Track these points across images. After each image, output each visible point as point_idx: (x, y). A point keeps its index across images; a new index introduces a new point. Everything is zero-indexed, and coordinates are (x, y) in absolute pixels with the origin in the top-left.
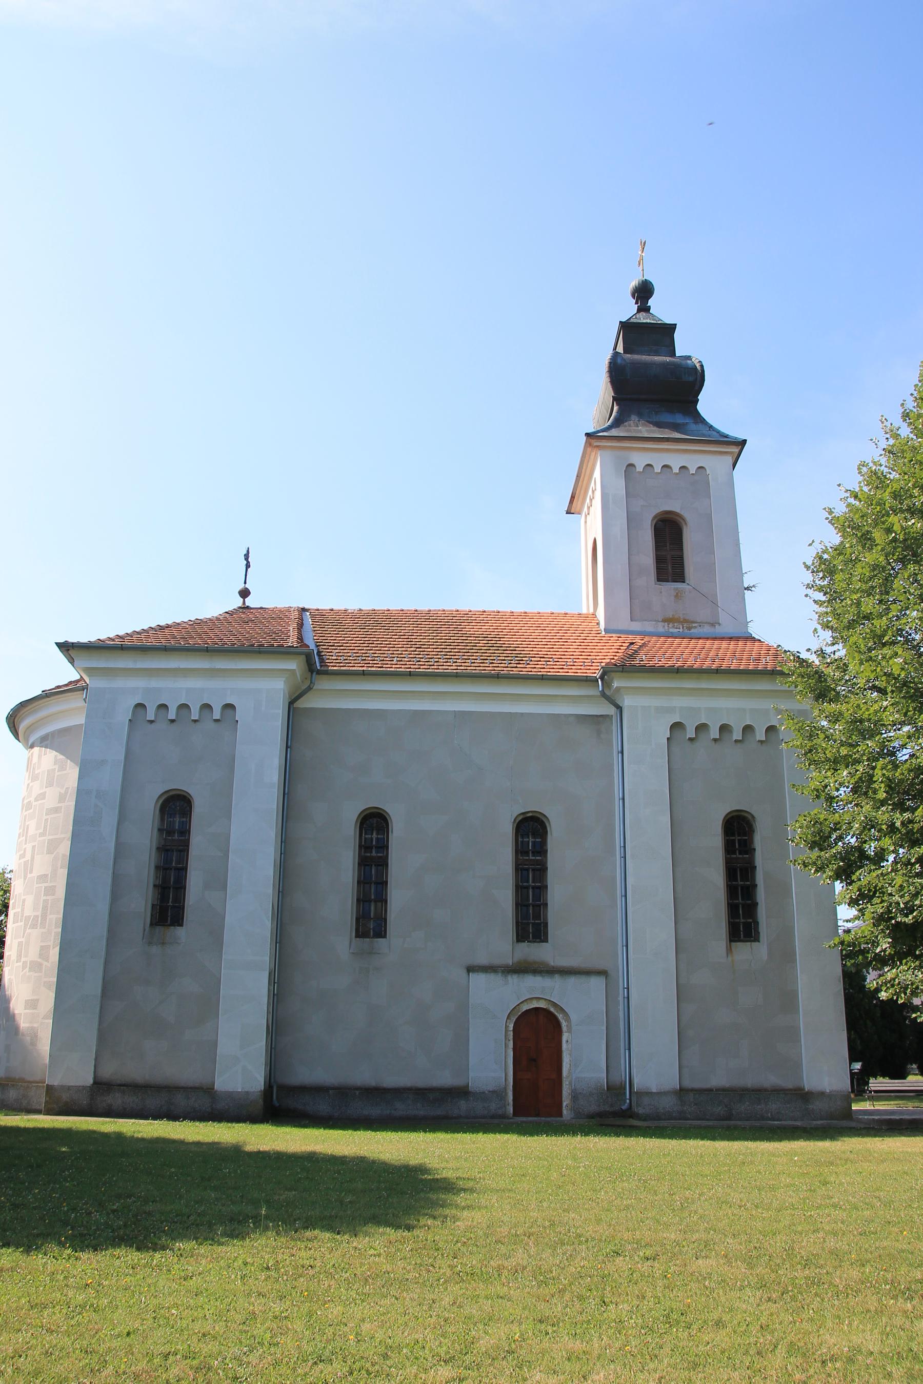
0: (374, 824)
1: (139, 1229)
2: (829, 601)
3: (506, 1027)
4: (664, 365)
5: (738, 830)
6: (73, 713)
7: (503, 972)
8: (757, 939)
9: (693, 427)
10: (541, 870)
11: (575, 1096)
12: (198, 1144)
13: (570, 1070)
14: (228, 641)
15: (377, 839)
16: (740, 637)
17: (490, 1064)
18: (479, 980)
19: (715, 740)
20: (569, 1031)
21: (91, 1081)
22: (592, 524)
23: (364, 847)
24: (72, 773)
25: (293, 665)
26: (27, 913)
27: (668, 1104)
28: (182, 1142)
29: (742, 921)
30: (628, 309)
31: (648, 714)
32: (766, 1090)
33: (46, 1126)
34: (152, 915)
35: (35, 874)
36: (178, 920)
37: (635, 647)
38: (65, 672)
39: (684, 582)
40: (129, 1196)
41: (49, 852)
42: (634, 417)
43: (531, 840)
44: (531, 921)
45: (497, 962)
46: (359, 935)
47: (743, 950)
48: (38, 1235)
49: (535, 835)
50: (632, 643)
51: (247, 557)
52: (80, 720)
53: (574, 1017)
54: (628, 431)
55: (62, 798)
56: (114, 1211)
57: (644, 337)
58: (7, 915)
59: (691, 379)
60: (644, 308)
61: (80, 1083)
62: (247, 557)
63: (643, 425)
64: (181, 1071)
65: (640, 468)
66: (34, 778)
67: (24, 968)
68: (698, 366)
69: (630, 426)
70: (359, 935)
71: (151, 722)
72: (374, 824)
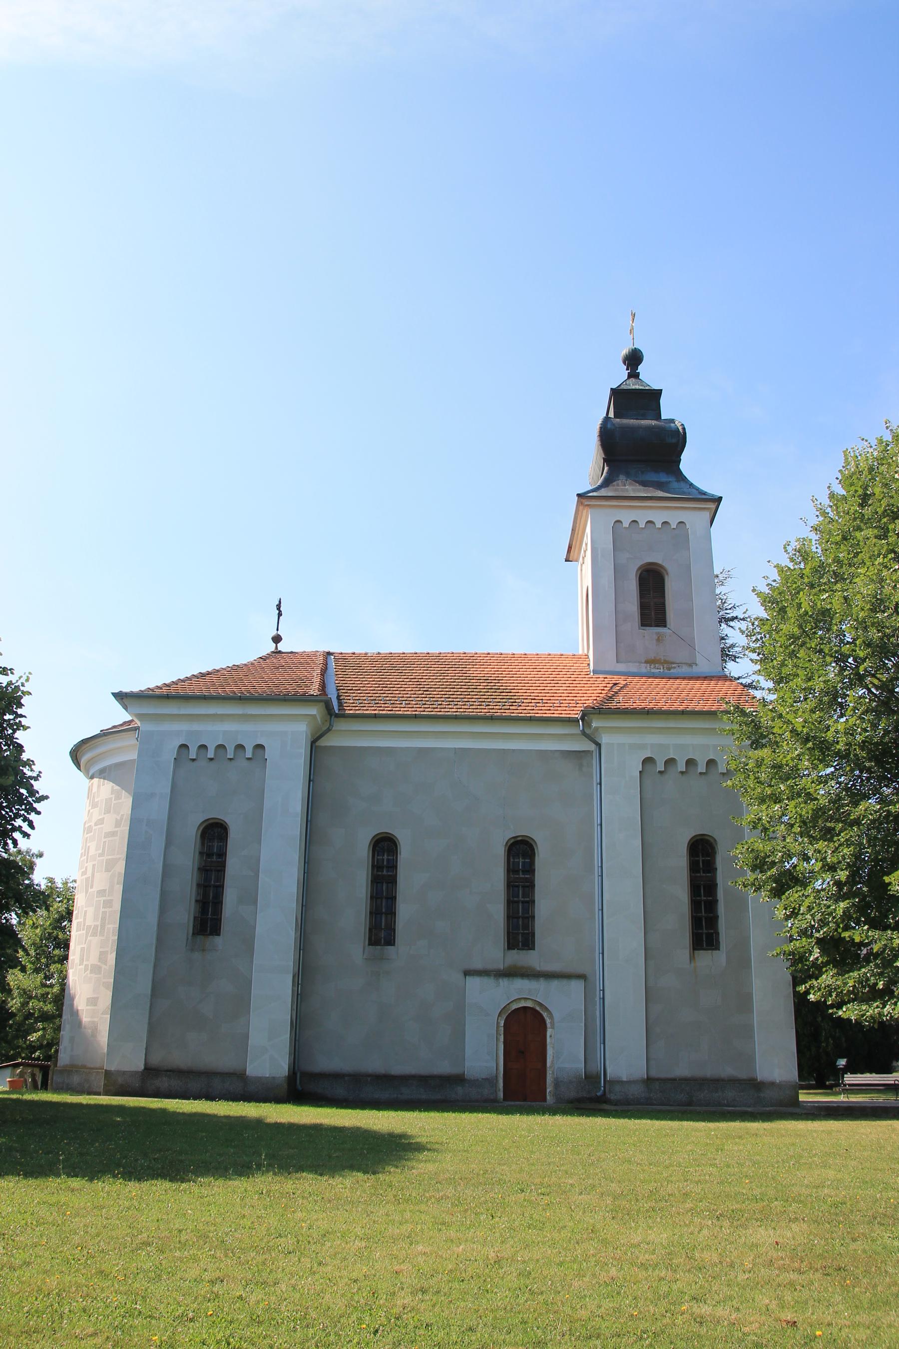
0: (385, 848)
1: (174, 1170)
2: (761, 660)
3: (498, 1023)
4: (649, 428)
5: (702, 852)
6: (127, 751)
7: (495, 976)
8: (718, 948)
9: (675, 485)
10: (530, 886)
11: (557, 1084)
12: (228, 1117)
13: (552, 1061)
14: (261, 689)
15: (388, 860)
16: (713, 677)
17: (483, 1054)
18: (473, 982)
19: (682, 773)
20: (553, 1027)
21: (143, 1067)
22: (584, 573)
23: (376, 867)
24: (126, 802)
25: (314, 711)
26: (88, 923)
27: (636, 1091)
28: (215, 1116)
29: (704, 931)
30: (619, 376)
31: (623, 751)
32: (723, 1080)
33: (105, 1103)
34: (194, 926)
35: (95, 889)
36: (216, 930)
37: (616, 689)
38: (119, 715)
39: (665, 626)
40: (168, 1150)
41: (107, 870)
42: (622, 477)
43: (521, 860)
44: (520, 930)
45: (490, 966)
46: (371, 943)
47: (705, 958)
48: (99, 1172)
49: (524, 856)
50: (615, 684)
51: (279, 607)
52: (134, 755)
53: (557, 1015)
54: (616, 490)
55: (118, 824)
56: (154, 1159)
57: (634, 402)
58: (70, 921)
59: (674, 441)
60: (634, 375)
61: (133, 1068)
62: (279, 607)
63: (630, 484)
64: (219, 1059)
65: (626, 524)
66: (94, 805)
67: (86, 970)
68: (680, 428)
69: (618, 485)
70: (371, 943)
71: (193, 760)
72: (385, 848)
